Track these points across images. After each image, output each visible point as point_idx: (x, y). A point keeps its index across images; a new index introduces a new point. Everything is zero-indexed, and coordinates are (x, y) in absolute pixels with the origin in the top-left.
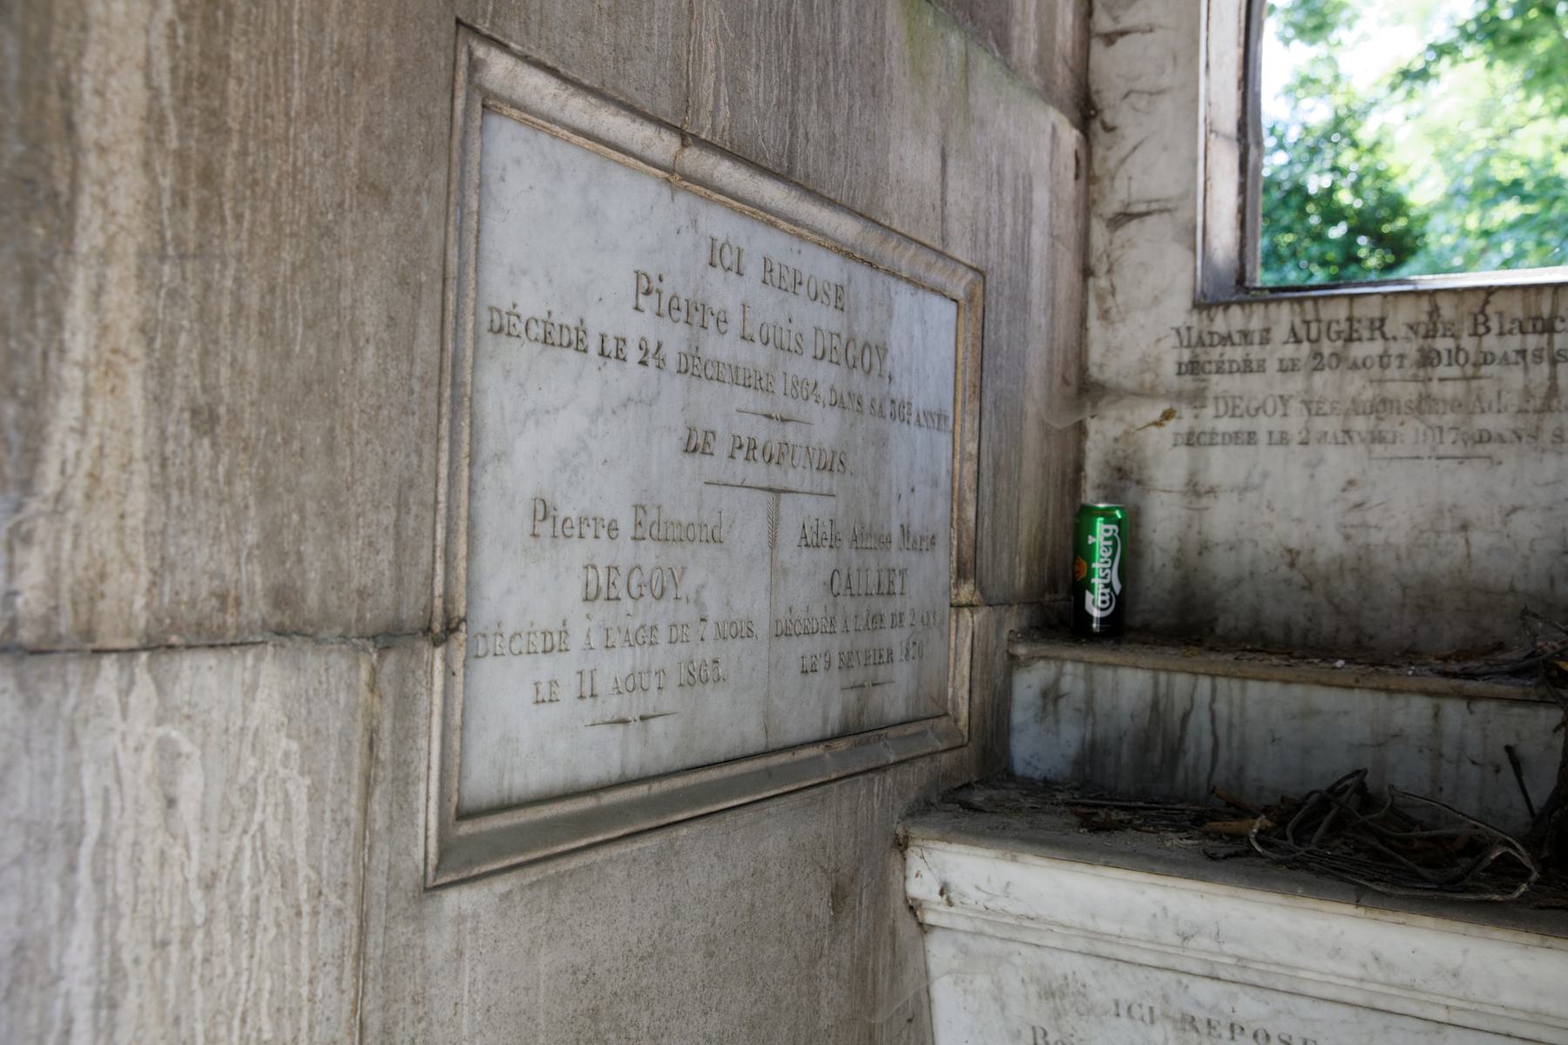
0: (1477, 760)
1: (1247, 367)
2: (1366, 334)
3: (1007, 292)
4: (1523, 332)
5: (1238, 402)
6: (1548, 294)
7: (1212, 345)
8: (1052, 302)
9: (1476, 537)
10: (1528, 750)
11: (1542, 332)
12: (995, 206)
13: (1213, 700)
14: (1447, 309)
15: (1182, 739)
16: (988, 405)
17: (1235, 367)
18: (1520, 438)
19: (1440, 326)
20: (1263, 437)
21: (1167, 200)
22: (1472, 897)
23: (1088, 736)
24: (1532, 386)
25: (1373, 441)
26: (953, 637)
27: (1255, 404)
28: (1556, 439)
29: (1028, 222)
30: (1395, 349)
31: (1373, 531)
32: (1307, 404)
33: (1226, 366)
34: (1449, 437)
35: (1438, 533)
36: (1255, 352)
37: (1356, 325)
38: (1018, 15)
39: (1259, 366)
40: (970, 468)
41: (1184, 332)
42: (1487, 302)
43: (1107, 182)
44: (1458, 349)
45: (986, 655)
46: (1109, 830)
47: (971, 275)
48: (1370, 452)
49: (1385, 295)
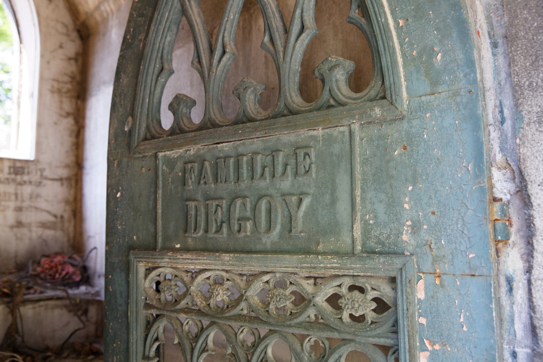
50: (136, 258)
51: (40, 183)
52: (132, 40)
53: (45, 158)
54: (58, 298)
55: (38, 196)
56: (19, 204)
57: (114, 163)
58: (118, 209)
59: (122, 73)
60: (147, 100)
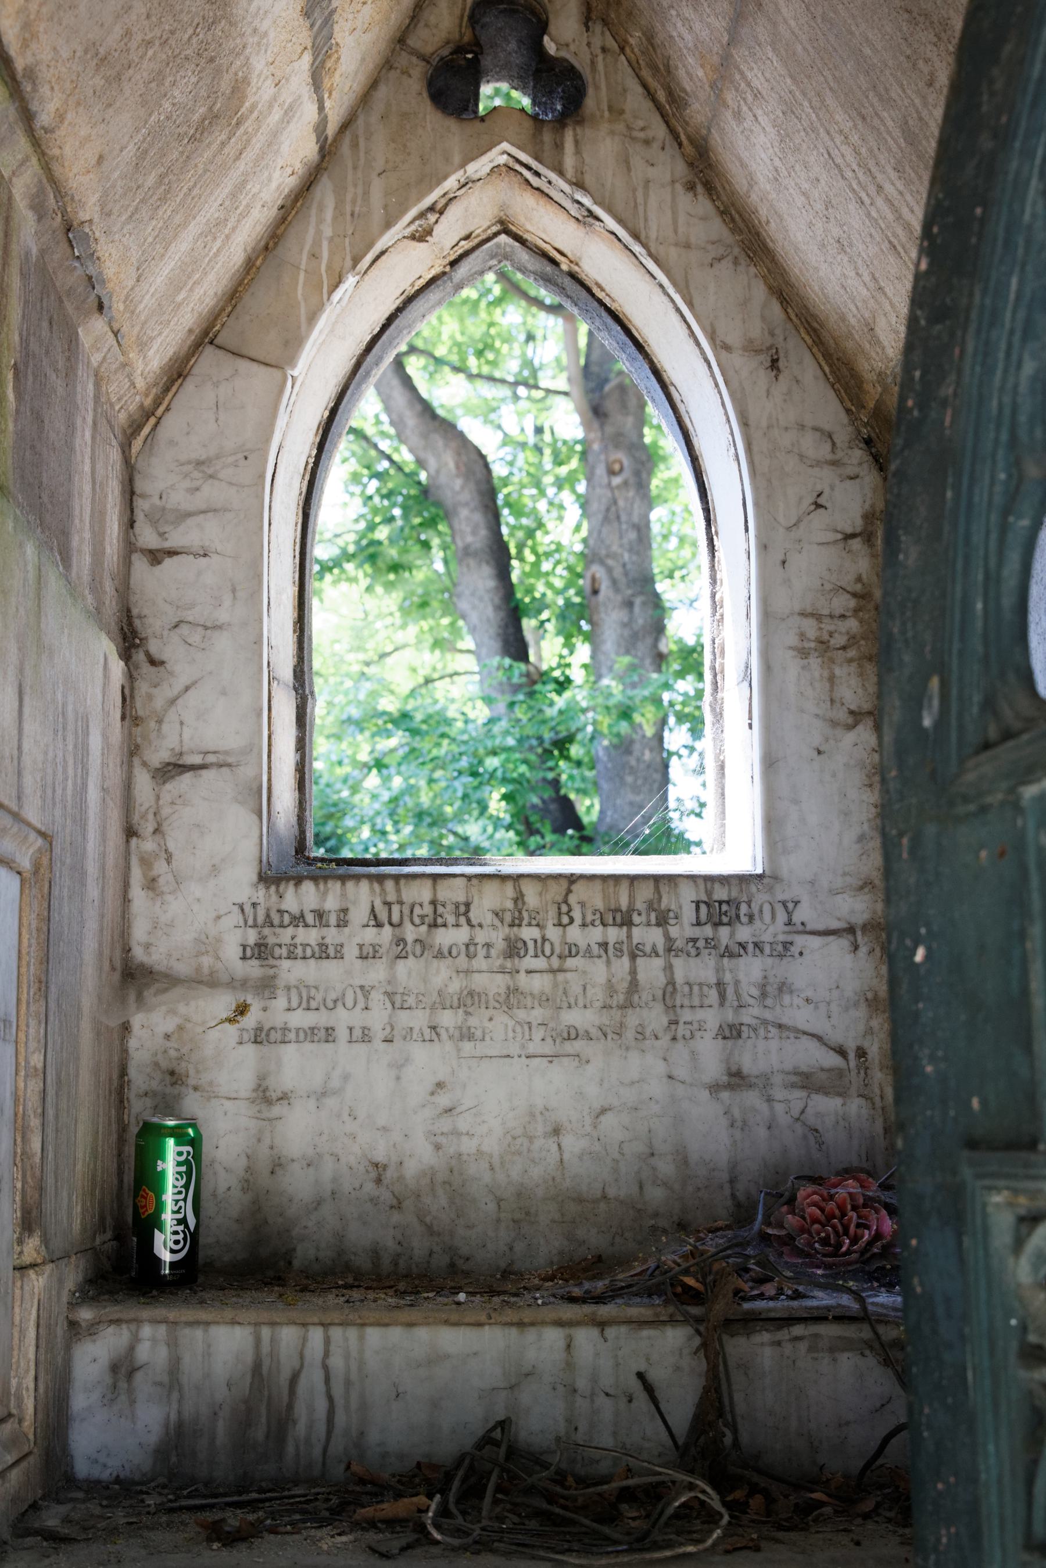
0: (611, 1392)
1: (323, 953)
2: (451, 919)
3: (68, 861)
4: (604, 924)
5: (313, 992)
6: (625, 886)
7: (282, 926)
8: (103, 868)
9: (568, 1141)
10: (657, 1375)
11: (621, 925)
12: (60, 754)
13: (327, 1354)
14: (532, 896)
15: (290, 1406)
16: (52, 1005)
17: (309, 952)
18: (605, 1035)
19: (525, 914)
20: (342, 1034)
21: (227, 753)
22: (668, 1553)
23: (173, 1416)
24: (614, 980)
25: (462, 1038)
26: (17, 1310)
27: (333, 995)
28: (640, 1037)
29: (85, 773)
30: (481, 937)
31: (465, 1139)
32: (390, 995)
33: (299, 951)
34: (538, 1034)
35: (531, 1139)
36: (332, 936)
37: (440, 909)
38: (77, 521)
39: (336, 951)
40: (34, 1086)
41: (248, 909)
42: (569, 891)
43: (153, 724)
44: (544, 939)
45: (49, 1327)
46: (244, 1539)
47: (40, 842)
48: (459, 1050)
49: (469, 878)
50: (979, 1176)
51: (787, 945)
52: (921, 410)
53: (795, 866)
54: (843, 1318)
55: (784, 988)
56: (730, 1016)
57: (900, 844)
58: (921, 1005)
59: (901, 532)
60: (979, 606)
